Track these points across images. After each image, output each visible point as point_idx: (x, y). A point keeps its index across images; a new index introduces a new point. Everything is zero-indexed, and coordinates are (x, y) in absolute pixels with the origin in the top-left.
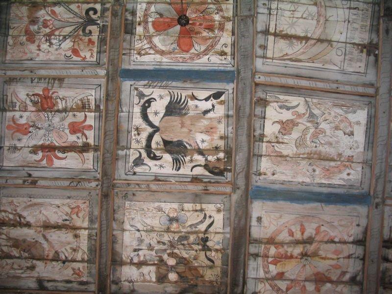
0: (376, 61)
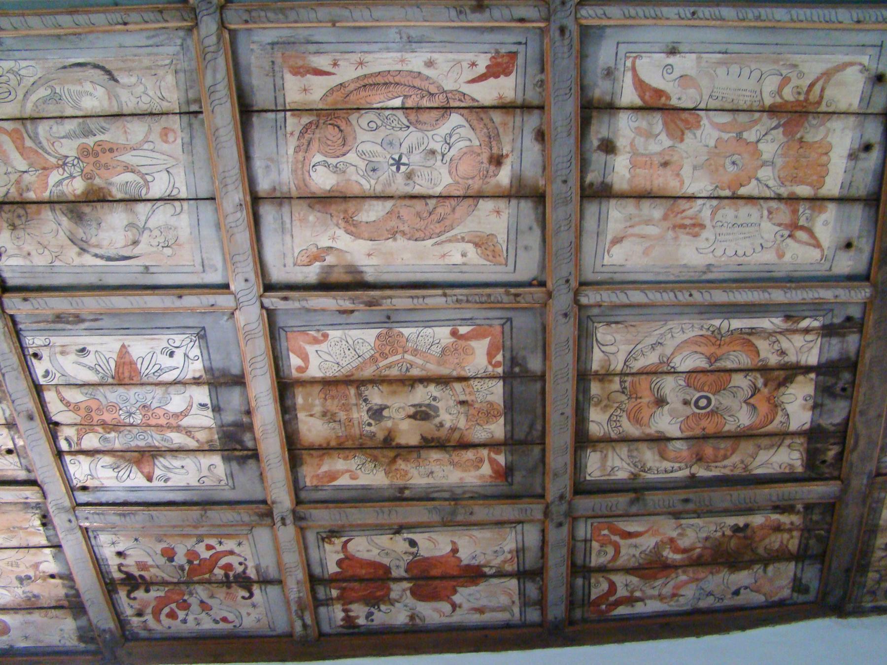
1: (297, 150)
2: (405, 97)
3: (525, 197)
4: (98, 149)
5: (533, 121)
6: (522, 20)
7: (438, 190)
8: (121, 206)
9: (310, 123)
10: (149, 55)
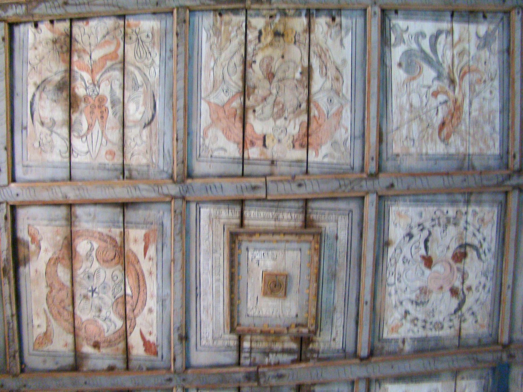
1: (101, 234)
2: (132, 297)
3: (76, 360)
4: (103, 109)
5: (120, 364)
6: (175, 360)
7: (78, 312)
8: (67, 118)
9: (116, 243)
10: (159, 150)
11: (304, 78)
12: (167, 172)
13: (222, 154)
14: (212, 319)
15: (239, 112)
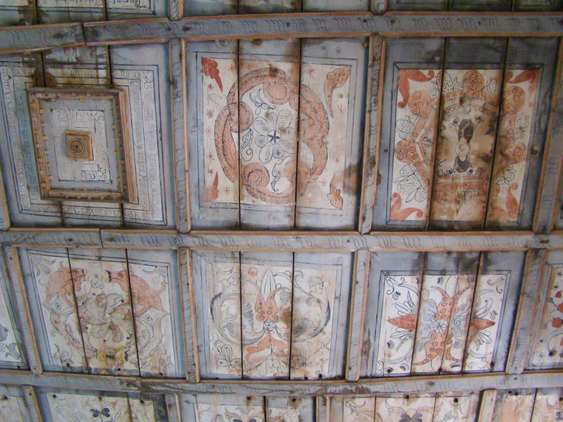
0: (13, 24)
4: (260, 310)
5: (247, 47)
6: (181, 56)
7: (294, 113)
8: (294, 304)
10: (206, 274)
11: (84, 324)
12: (198, 254)
13: (147, 268)
14: (142, 104)
15: (136, 301)
